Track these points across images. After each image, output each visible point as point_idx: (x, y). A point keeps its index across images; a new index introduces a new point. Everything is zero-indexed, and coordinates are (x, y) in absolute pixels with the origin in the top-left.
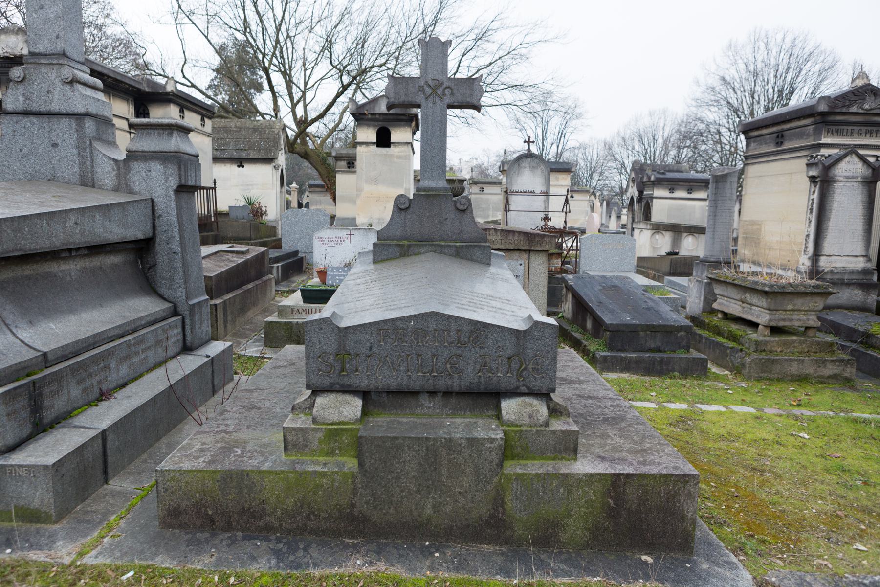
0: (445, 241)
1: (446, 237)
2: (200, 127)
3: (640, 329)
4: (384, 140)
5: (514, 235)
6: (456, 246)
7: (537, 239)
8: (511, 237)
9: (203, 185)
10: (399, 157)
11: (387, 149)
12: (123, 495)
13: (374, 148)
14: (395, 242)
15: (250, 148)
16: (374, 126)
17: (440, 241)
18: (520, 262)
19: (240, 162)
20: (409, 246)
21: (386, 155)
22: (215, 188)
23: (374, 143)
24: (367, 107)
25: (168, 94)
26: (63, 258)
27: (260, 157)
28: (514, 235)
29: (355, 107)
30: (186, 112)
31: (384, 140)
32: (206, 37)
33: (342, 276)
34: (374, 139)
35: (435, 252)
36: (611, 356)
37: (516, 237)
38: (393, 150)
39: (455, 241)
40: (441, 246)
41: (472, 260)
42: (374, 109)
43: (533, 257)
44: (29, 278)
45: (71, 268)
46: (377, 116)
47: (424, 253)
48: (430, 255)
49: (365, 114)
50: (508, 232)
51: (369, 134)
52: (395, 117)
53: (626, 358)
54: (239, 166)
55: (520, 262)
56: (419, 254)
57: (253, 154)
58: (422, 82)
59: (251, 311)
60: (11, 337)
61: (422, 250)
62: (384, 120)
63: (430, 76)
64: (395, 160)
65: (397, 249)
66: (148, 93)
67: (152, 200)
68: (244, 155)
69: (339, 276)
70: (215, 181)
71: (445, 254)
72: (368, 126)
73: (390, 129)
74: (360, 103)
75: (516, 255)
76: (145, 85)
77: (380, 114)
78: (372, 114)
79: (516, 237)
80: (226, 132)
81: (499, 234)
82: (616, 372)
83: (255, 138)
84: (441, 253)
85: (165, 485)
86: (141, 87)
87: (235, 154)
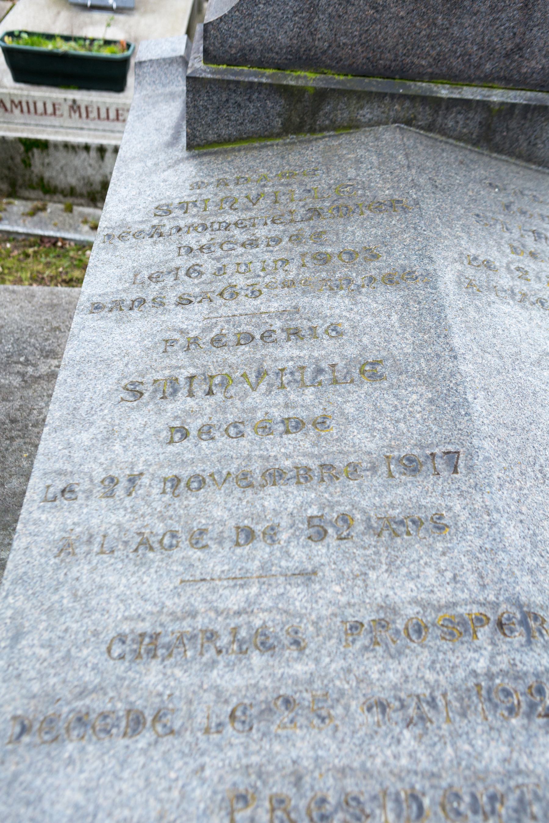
0: (454, 78)
1: (456, 63)
6: (485, 105)
12: (372, 764)
14: (267, 76)
17: (433, 78)
20: (322, 95)
35: (409, 122)
39: (488, 81)
40: (437, 103)
41: (529, 158)
47: (371, 124)
48: (389, 135)
56: (353, 126)
59: (68, 347)
61: (366, 113)
65: (275, 106)
71: (443, 132)
84: (429, 128)
85: (524, 713)
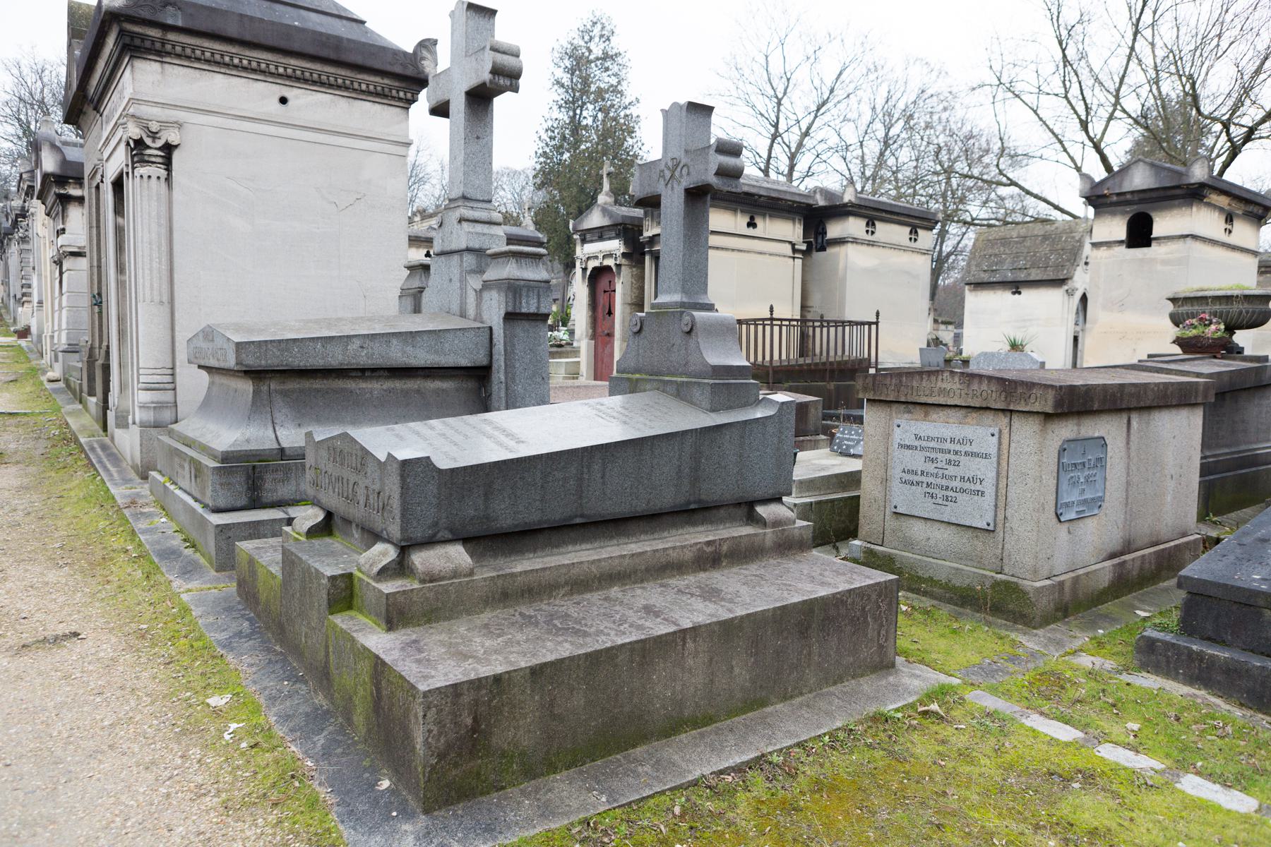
2: (907, 243)
3: (1261, 602)
4: (1140, 235)
5: (980, 383)
7: (1020, 390)
8: (975, 386)
9: (850, 316)
10: (1165, 262)
11: (1145, 250)
13: (1123, 248)
15: (1032, 266)
16: (1124, 213)
18: (991, 430)
19: (1016, 287)
21: (1142, 260)
22: (877, 323)
23: (1122, 242)
24: (1109, 184)
25: (845, 205)
26: (352, 377)
27: (1045, 278)
28: (980, 383)
29: (1088, 186)
30: (879, 225)
31: (1140, 235)
32: (1035, 112)
33: (852, 440)
34: (1121, 233)
36: (1166, 643)
37: (984, 386)
38: (1155, 250)
42: (1120, 186)
43: (1017, 422)
44: (318, 391)
45: (376, 387)
46: (1129, 197)
49: (1105, 196)
50: (972, 376)
51: (1116, 228)
52: (1162, 193)
53: (1200, 656)
54: (1014, 293)
55: (991, 430)
57: (1035, 275)
58: (662, 167)
60: (270, 433)
62: (1141, 201)
63: (670, 155)
64: (1159, 267)
66: (825, 207)
67: (491, 328)
68: (1022, 276)
69: (848, 440)
70: (878, 314)
72: (1113, 214)
73: (1153, 215)
74: (1097, 180)
75: (988, 417)
76: (818, 196)
77: (1132, 192)
78: (1118, 194)
79: (984, 386)
80: (1003, 245)
81: (957, 379)
82: (1175, 679)
83: (1045, 248)
86: (811, 202)
87: (1010, 276)
